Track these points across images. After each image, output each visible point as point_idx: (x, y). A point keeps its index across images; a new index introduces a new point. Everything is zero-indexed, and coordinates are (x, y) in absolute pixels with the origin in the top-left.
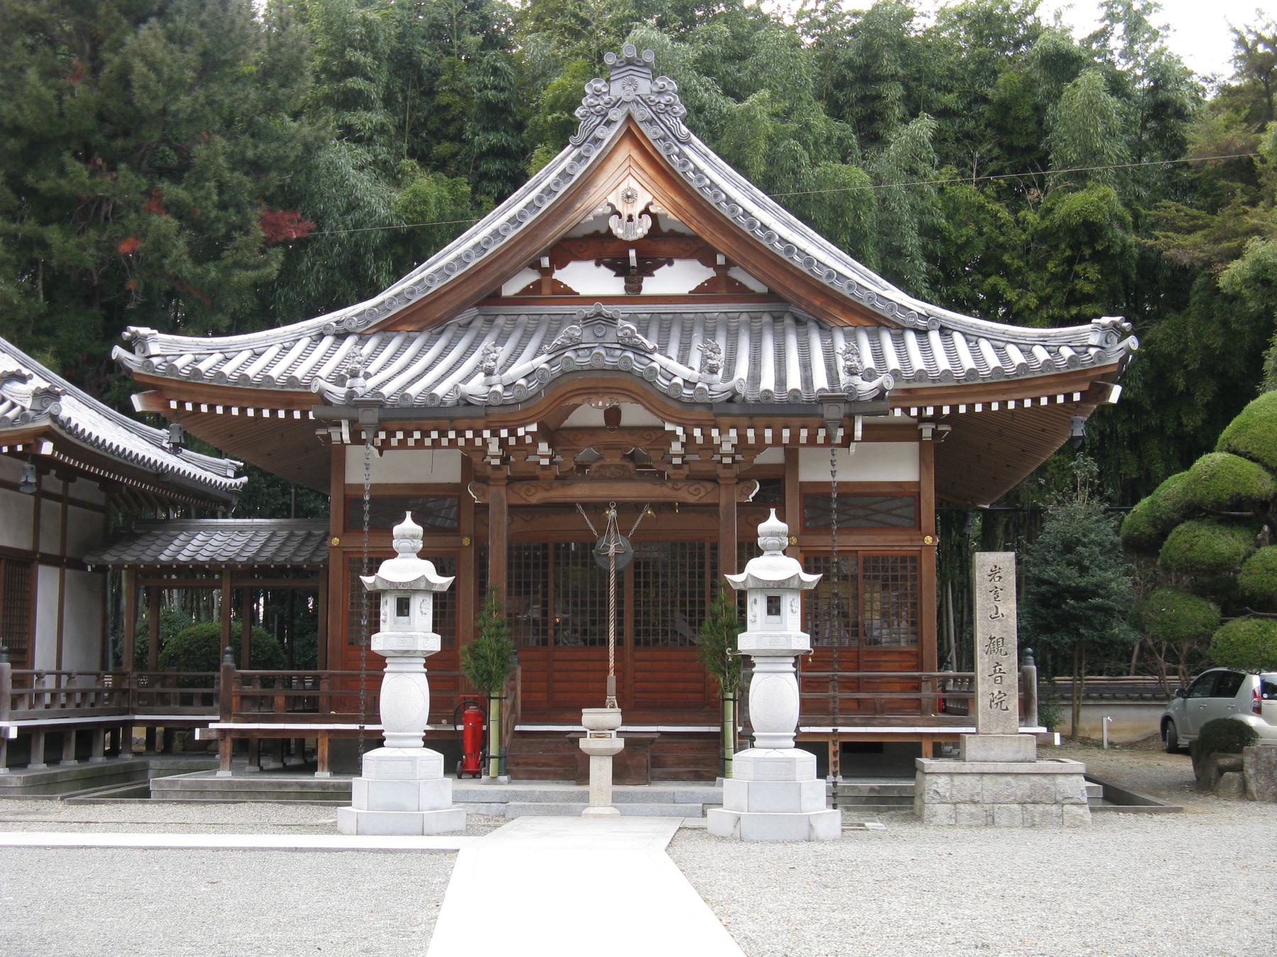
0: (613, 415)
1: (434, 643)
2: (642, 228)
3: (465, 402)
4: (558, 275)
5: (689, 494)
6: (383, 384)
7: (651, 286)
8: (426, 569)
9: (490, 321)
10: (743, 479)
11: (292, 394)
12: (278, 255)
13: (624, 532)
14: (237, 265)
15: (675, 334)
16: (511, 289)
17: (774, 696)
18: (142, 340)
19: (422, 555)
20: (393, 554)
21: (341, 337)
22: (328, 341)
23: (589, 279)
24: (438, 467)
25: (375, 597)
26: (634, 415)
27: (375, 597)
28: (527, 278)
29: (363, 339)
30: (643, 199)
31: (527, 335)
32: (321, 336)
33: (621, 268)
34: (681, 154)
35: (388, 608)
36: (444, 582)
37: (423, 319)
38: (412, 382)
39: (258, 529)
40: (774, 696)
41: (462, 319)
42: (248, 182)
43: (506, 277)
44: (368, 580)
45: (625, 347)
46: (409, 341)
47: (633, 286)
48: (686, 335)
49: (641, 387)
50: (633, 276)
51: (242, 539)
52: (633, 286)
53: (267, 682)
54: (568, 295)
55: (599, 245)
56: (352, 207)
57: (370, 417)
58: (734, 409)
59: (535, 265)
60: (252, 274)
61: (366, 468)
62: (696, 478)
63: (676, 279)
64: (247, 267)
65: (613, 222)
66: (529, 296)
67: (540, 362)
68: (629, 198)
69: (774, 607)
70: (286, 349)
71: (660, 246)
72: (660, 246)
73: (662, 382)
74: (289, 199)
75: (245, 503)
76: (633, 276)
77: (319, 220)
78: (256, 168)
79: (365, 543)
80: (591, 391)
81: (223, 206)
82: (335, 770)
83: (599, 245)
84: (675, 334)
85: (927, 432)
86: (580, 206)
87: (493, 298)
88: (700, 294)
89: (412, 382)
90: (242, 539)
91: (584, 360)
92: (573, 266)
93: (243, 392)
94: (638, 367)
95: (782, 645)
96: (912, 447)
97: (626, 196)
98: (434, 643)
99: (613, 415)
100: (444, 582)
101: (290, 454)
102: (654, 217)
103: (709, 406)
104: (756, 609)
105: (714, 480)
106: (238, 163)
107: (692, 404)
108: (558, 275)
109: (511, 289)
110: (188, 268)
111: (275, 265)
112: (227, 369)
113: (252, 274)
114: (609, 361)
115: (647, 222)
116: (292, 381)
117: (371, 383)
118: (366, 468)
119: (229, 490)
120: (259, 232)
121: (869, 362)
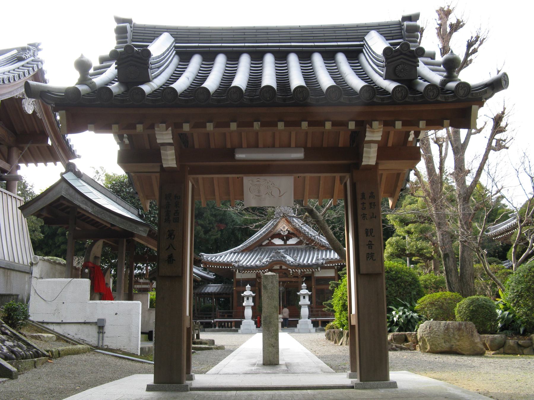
0: (281, 267)
1: (253, 304)
2: (286, 233)
3: (256, 266)
4: (272, 241)
5: (293, 280)
6: (243, 263)
7: (289, 242)
8: (251, 293)
9: (261, 249)
10: (303, 277)
11: (228, 264)
12: (220, 233)
13: (283, 286)
14: (212, 235)
15: (292, 251)
16: (264, 244)
17: (305, 311)
18: (203, 255)
19: (250, 291)
20: (246, 291)
21: (235, 253)
22: (232, 254)
23: (278, 242)
24: (252, 275)
25: (243, 297)
26: (284, 267)
27: (243, 297)
28: (267, 242)
29: (239, 253)
30: (286, 228)
31: (267, 252)
32: (231, 253)
33: (283, 239)
34: (293, 220)
35: (245, 299)
36: (254, 295)
37: (249, 250)
38: (248, 262)
39: (216, 286)
40: (305, 311)
41: (256, 249)
42: (214, 219)
43: (263, 242)
44: (242, 295)
45: (282, 257)
46: (247, 254)
47: (285, 242)
48: (294, 251)
49: (285, 263)
50: (285, 241)
51: (216, 288)
52: (285, 242)
53: (223, 313)
54: (274, 244)
55: (279, 236)
56: (233, 221)
57: (241, 269)
58: (299, 266)
59: (268, 239)
60: (215, 237)
61: (239, 276)
62: (294, 277)
63: (292, 241)
64: (214, 235)
65: (281, 232)
66: (267, 245)
67: (268, 259)
68: (284, 228)
69: (304, 297)
70: (226, 256)
71: (290, 236)
72: (290, 236)
73: (288, 262)
74: (221, 221)
75: (214, 281)
76: (285, 241)
77: (227, 224)
78: (215, 216)
79: (241, 289)
80: (276, 264)
81: (209, 224)
82: (236, 327)
83: (279, 236)
84: (292, 251)
85: (336, 268)
86: (276, 229)
87: (261, 245)
88: (297, 244)
89: (248, 262)
90: (216, 288)
91: (275, 259)
92: (275, 239)
93: (220, 264)
94: (284, 260)
95: (305, 303)
96: (333, 270)
97: (283, 227)
98: (253, 304)
99: (281, 267)
100: (254, 295)
101: (225, 274)
102: (289, 231)
103: (295, 266)
104: (302, 298)
105: (297, 277)
106: (212, 215)
107: (292, 266)
108: (272, 241)
109: (264, 244)
110: (203, 236)
111: (219, 235)
112: (217, 260)
113: (215, 237)
114: (279, 259)
115: (287, 232)
116: (228, 262)
117: (241, 263)
118: (239, 276)
119: (212, 279)
120: (216, 229)
121: (324, 257)
